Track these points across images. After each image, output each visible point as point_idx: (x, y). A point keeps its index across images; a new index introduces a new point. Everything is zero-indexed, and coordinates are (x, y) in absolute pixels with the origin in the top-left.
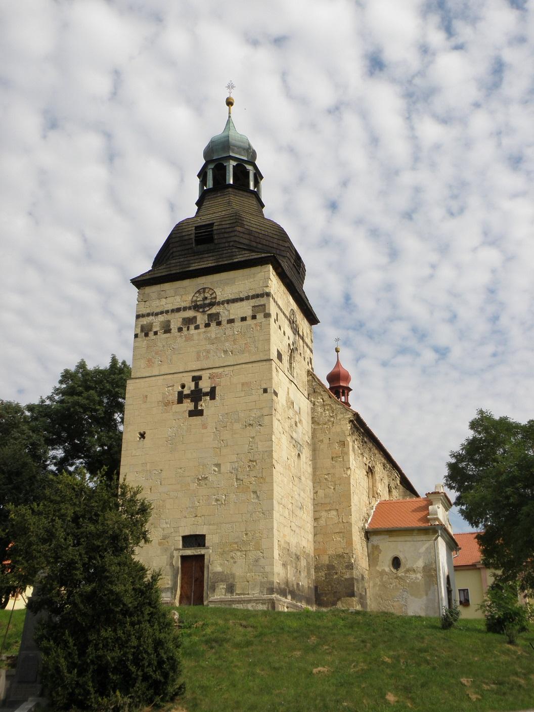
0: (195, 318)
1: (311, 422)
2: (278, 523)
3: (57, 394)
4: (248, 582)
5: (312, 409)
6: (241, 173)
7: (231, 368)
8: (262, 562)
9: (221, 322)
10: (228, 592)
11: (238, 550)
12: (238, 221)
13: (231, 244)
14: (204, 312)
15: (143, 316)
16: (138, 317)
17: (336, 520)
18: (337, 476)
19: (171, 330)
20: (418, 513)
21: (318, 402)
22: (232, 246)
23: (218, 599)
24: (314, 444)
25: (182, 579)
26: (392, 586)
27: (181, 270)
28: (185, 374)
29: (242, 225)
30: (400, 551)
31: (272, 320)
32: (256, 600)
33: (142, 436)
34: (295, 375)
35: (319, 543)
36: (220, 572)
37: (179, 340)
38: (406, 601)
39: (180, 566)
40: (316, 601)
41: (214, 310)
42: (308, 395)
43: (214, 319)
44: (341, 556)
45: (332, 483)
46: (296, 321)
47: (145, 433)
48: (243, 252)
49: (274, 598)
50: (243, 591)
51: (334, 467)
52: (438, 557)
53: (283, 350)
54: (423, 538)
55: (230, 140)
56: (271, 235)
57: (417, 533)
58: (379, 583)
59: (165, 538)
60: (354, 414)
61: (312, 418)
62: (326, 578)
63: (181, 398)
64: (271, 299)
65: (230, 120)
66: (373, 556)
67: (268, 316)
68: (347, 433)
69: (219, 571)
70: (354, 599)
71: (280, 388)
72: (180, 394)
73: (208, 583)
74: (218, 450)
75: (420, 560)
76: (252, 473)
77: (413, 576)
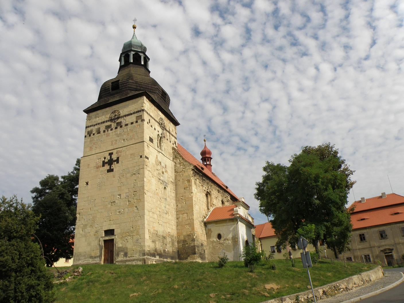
0: (111, 125)
1: (174, 172)
2: (148, 221)
3: (75, 171)
4: (133, 251)
5: (175, 165)
6: (137, 57)
7: (125, 148)
8: (140, 240)
9: (122, 126)
10: (125, 256)
11: (129, 236)
12: (130, 77)
13: (127, 89)
14: (115, 122)
15: (89, 127)
16: (86, 127)
17: (186, 218)
18: (187, 197)
19: (100, 132)
20: (230, 212)
22: (128, 89)
23: (120, 260)
24: (176, 182)
25: (105, 251)
27: (105, 103)
28: (105, 152)
29: (132, 79)
30: (221, 231)
31: (145, 123)
32: (137, 259)
33: (87, 183)
34: (163, 149)
36: (121, 247)
37: (104, 136)
39: (103, 245)
40: (178, 258)
41: (119, 121)
42: (173, 159)
43: (119, 125)
44: (189, 235)
45: (185, 200)
46: (164, 124)
47: (88, 182)
48: (132, 92)
49: (145, 258)
50: (131, 255)
51: (185, 193)
52: (239, 232)
53: (154, 137)
54: (232, 223)
55: (132, 43)
58: (212, 247)
59: (96, 232)
61: (175, 170)
62: (183, 246)
63: (104, 164)
64: (145, 112)
65: (134, 35)
66: (208, 235)
67: (143, 120)
68: (191, 176)
69: (120, 246)
70: (196, 255)
71: (150, 155)
72: (104, 162)
73: (115, 252)
74: (120, 188)
76: (135, 198)
77: (227, 242)
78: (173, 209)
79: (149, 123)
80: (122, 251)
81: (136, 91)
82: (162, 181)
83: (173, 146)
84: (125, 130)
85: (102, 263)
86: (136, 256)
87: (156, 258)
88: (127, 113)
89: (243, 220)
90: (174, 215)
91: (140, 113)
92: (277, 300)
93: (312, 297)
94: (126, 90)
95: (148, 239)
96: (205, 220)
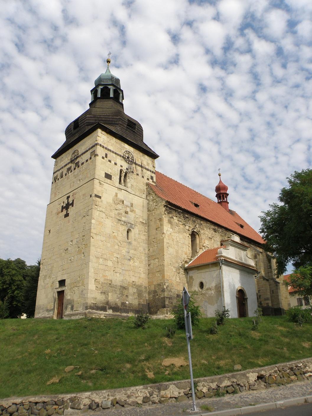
1: (147, 211)
8: (84, 292)
17: (157, 264)
21: (150, 199)
26: (199, 299)
30: (203, 278)
32: (80, 313)
35: (150, 278)
38: (206, 308)
47: (50, 230)
51: (157, 234)
56: (107, 115)
57: (211, 266)
60: (166, 202)
61: (148, 208)
62: (153, 298)
68: (163, 213)
75: (214, 282)
77: (210, 292)
78: (143, 255)
79: (105, 158)
80: (70, 304)
81: (92, 125)
82: (125, 222)
83: (148, 181)
84: (81, 170)
85: (55, 318)
86: (80, 310)
87: (107, 312)
88: (84, 151)
89: (232, 264)
90: (144, 261)
91: (94, 148)
92: (149, 388)
93: (228, 386)
94: (85, 126)
95: (95, 289)
96: (186, 265)
